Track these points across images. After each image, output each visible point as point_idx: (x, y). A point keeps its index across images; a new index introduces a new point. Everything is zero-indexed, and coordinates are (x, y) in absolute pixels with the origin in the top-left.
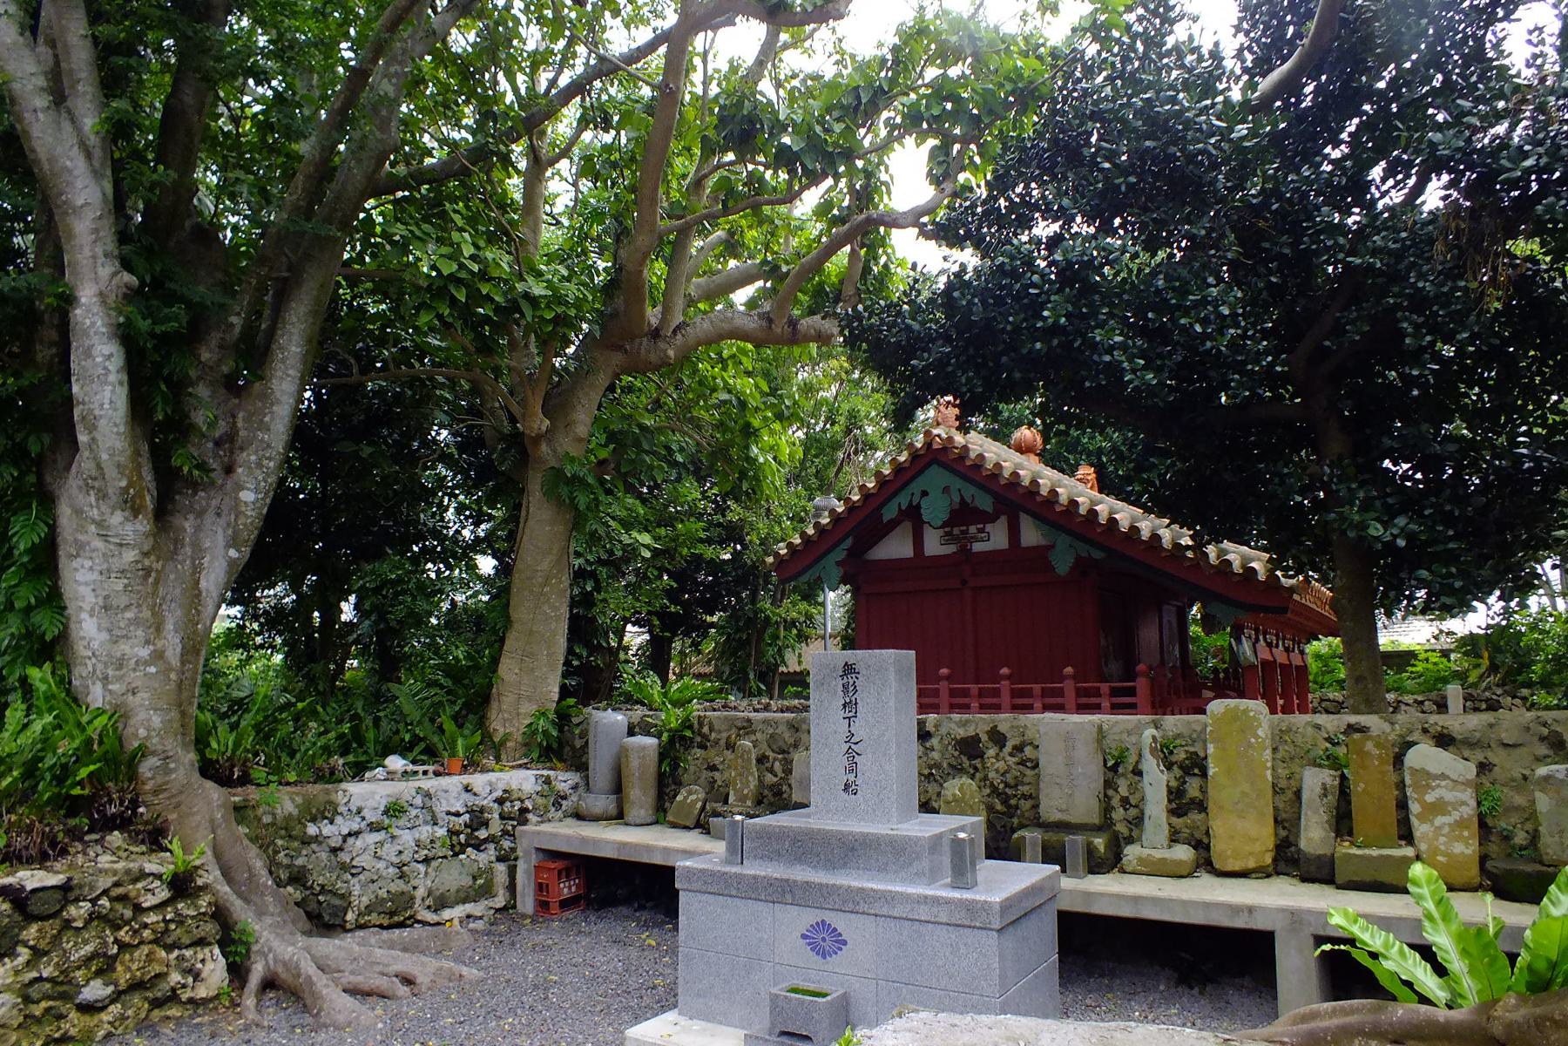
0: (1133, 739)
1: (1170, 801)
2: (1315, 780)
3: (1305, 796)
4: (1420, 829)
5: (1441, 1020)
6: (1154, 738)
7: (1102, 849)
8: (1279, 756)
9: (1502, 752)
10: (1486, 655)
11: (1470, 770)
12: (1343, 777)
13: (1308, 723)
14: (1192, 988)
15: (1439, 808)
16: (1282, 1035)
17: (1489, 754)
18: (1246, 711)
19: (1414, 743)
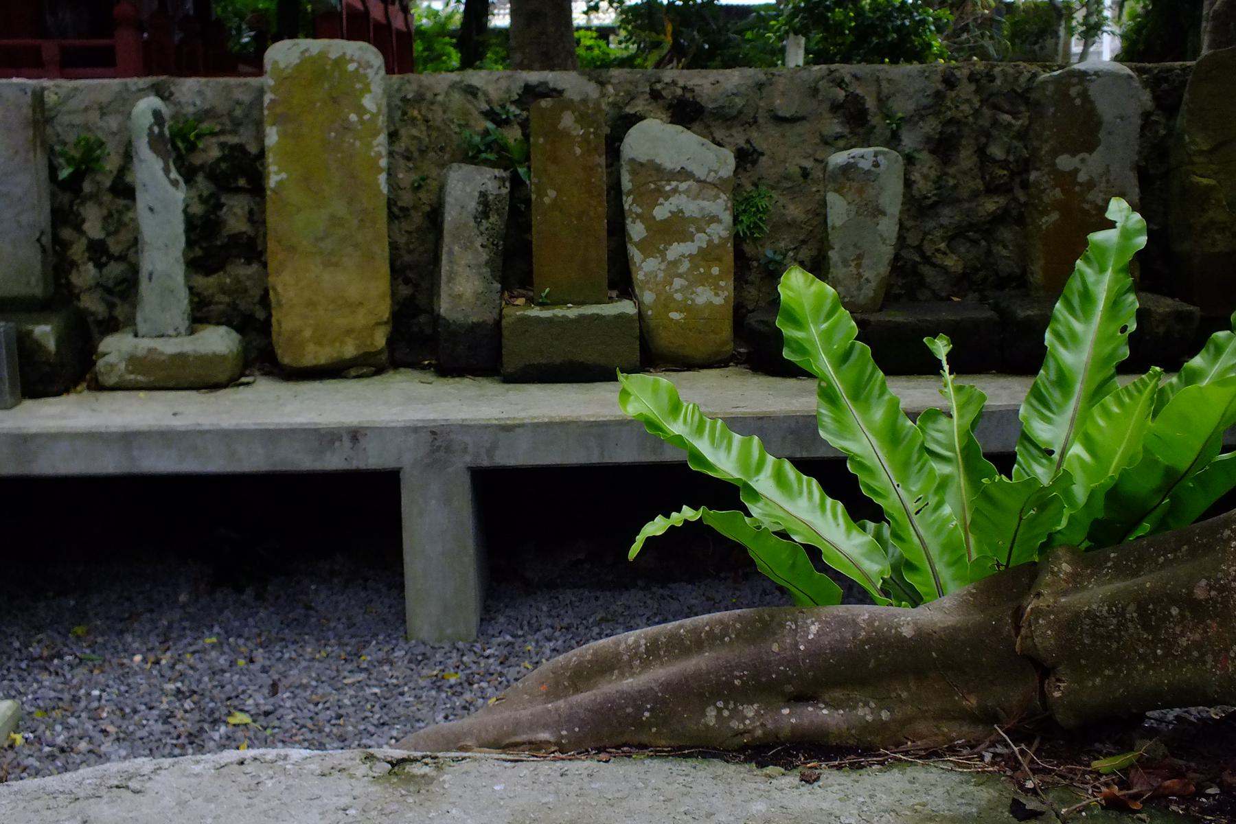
0: (113, 123)
1: (190, 244)
2: (466, 188)
3: (451, 216)
4: (645, 267)
5: (907, 632)
6: (157, 114)
7: (51, 345)
8: (400, 147)
9: (773, 131)
10: (669, 28)
11: (721, 162)
12: (516, 181)
13: (453, 86)
14: (239, 590)
15: (676, 228)
16: (533, 725)
17: (754, 135)
18: (340, 62)
19: (637, 118)
